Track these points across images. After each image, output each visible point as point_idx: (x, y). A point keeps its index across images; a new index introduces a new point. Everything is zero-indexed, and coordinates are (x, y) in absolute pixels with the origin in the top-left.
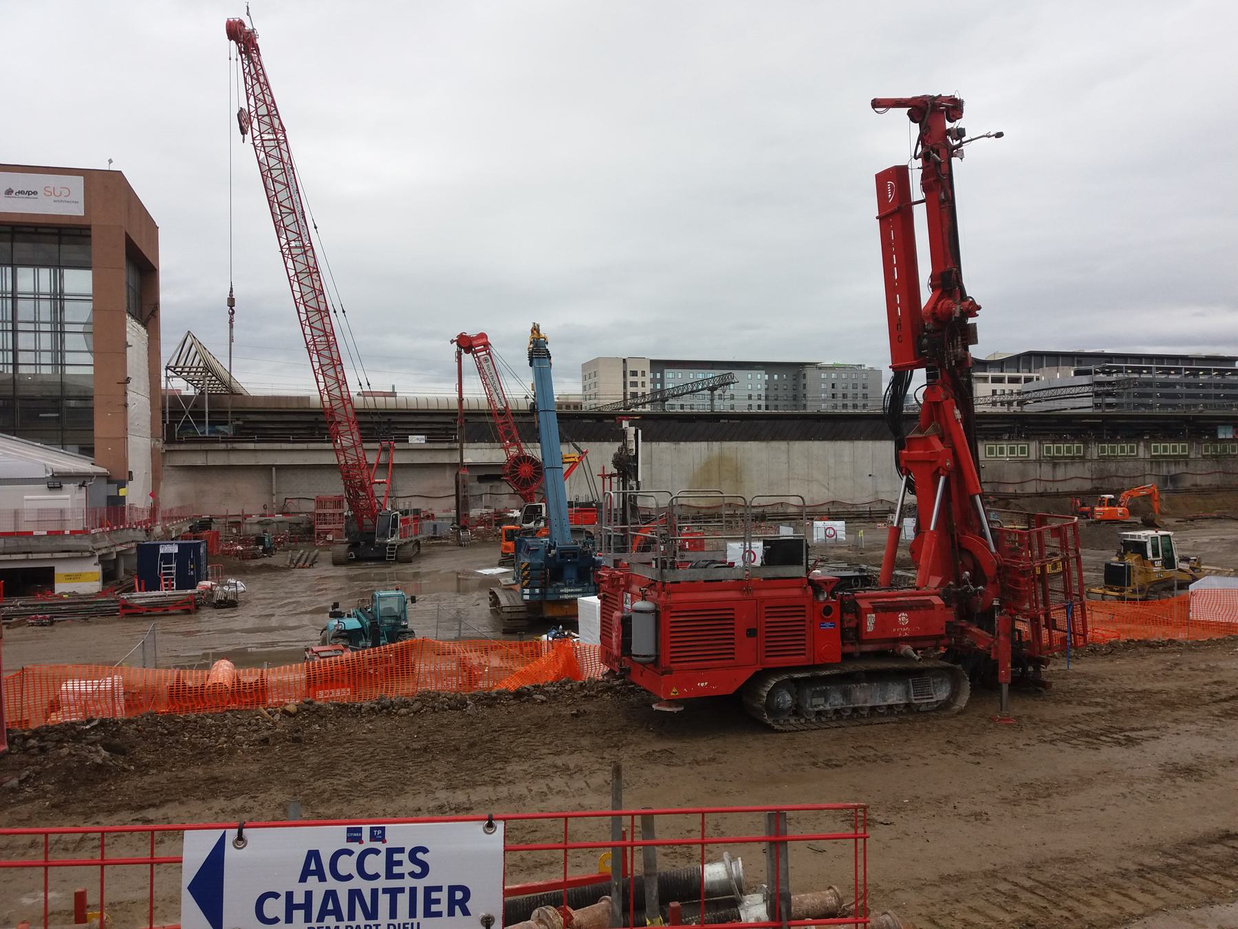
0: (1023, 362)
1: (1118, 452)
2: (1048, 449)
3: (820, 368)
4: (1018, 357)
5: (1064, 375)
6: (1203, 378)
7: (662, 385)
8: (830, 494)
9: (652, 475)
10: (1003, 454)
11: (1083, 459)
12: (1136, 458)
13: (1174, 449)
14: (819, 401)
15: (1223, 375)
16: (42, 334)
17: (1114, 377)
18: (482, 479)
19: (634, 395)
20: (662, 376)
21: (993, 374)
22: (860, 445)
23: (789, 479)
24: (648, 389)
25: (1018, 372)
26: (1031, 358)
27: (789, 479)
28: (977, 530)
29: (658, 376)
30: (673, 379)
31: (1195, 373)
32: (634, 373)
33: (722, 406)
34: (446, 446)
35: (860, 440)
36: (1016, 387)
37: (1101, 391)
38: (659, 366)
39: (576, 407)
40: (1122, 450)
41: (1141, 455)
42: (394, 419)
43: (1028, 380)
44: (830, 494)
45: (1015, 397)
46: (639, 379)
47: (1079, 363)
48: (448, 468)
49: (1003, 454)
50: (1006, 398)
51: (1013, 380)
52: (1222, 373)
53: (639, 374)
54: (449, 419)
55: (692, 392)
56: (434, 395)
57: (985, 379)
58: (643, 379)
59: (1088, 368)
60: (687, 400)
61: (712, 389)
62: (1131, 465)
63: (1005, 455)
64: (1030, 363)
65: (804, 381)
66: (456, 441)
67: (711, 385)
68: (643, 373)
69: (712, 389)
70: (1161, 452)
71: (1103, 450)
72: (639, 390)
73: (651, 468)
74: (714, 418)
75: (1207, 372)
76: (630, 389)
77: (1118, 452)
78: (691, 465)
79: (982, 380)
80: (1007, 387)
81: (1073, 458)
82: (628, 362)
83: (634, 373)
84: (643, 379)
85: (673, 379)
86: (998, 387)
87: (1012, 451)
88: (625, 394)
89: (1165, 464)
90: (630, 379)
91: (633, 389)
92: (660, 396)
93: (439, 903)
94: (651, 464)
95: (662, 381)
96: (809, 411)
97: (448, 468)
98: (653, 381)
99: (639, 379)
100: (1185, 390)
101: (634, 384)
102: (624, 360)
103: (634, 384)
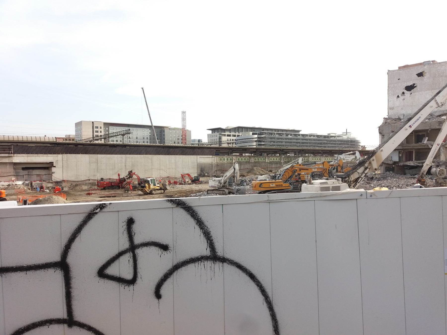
0: (237, 130)
1: (260, 160)
2: (239, 159)
3: (170, 129)
4: (235, 128)
5: (147, 133)
6: (289, 136)
7: (109, 132)
8: (167, 174)
9: (98, 167)
10: (225, 160)
11: (249, 162)
12: (265, 162)
13: (274, 159)
14: (169, 141)
15: (296, 136)
16: (347, 132)
17: (262, 136)
18: (24, 169)
19: (97, 136)
20: (108, 129)
21: (237, 134)
22: (178, 156)
23: (152, 169)
24: (103, 134)
25: (235, 133)
26: (239, 129)
27: (152, 169)
28: (369, 166)
29: (107, 129)
30: (112, 130)
31: (287, 135)
32: (97, 127)
33: (126, 141)
34: (7, 155)
35: (178, 155)
36: (234, 138)
37: (259, 140)
38: (107, 125)
39: (73, 140)
40: (261, 160)
41: (267, 161)
42: (19, 144)
43: (238, 136)
44: (167, 174)
45: (234, 141)
46: (99, 130)
47: (254, 131)
48: (8, 164)
49: (225, 160)
50: (232, 141)
51: (235, 136)
52: (295, 135)
53: (99, 128)
54: (9, 144)
55: (116, 136)
56: (34, 135)
57: (225, 135)
58: (101, 130)
59: (256, 132)
60: (115, 139)
61: (123, 135)
62: (263, 164)
63: (225, 161)
64: (239, 130)
65: (163, 133)
66: (11, 153)
67: (122, 133)
68: (101, 128)
69: (123, 135)
70: (272, 160)
71: (255, 160)
72: (99, 134)
73: (97, 165)
74: (125, 146)
75: (291, 135)
76: (95, 134)
77: (260, 160)
78: (114, 163)
79: (223, 135)
80: (232, 138)
81: (246, 162)
82: (94, 123)
83: (97, 127)
84: (101, 130)
85: (112, 130)
86: (229, 138)
87: (227, 160)
88: (93, 135)
89: (273, 164)
90: (95, 130)
91: (97, 134)
92: (107, 136)
93: (101, 131)
94: (97, 163)
95: (108, 131)
96: (166, 144)
97: (8, 164)
98: (105, 131)
99: (99, 130)
100: (269, 140)
101: (97, 132)
102: (93, 122)
103: (97, 132)
